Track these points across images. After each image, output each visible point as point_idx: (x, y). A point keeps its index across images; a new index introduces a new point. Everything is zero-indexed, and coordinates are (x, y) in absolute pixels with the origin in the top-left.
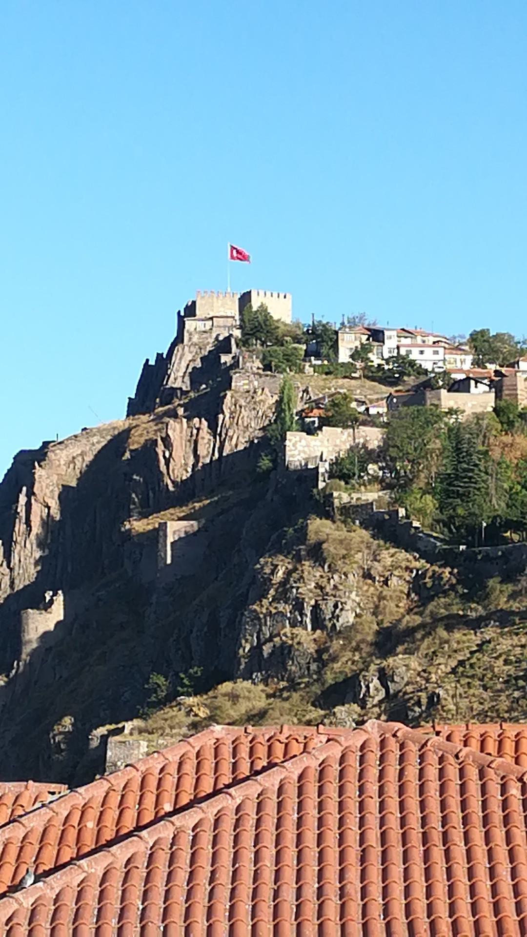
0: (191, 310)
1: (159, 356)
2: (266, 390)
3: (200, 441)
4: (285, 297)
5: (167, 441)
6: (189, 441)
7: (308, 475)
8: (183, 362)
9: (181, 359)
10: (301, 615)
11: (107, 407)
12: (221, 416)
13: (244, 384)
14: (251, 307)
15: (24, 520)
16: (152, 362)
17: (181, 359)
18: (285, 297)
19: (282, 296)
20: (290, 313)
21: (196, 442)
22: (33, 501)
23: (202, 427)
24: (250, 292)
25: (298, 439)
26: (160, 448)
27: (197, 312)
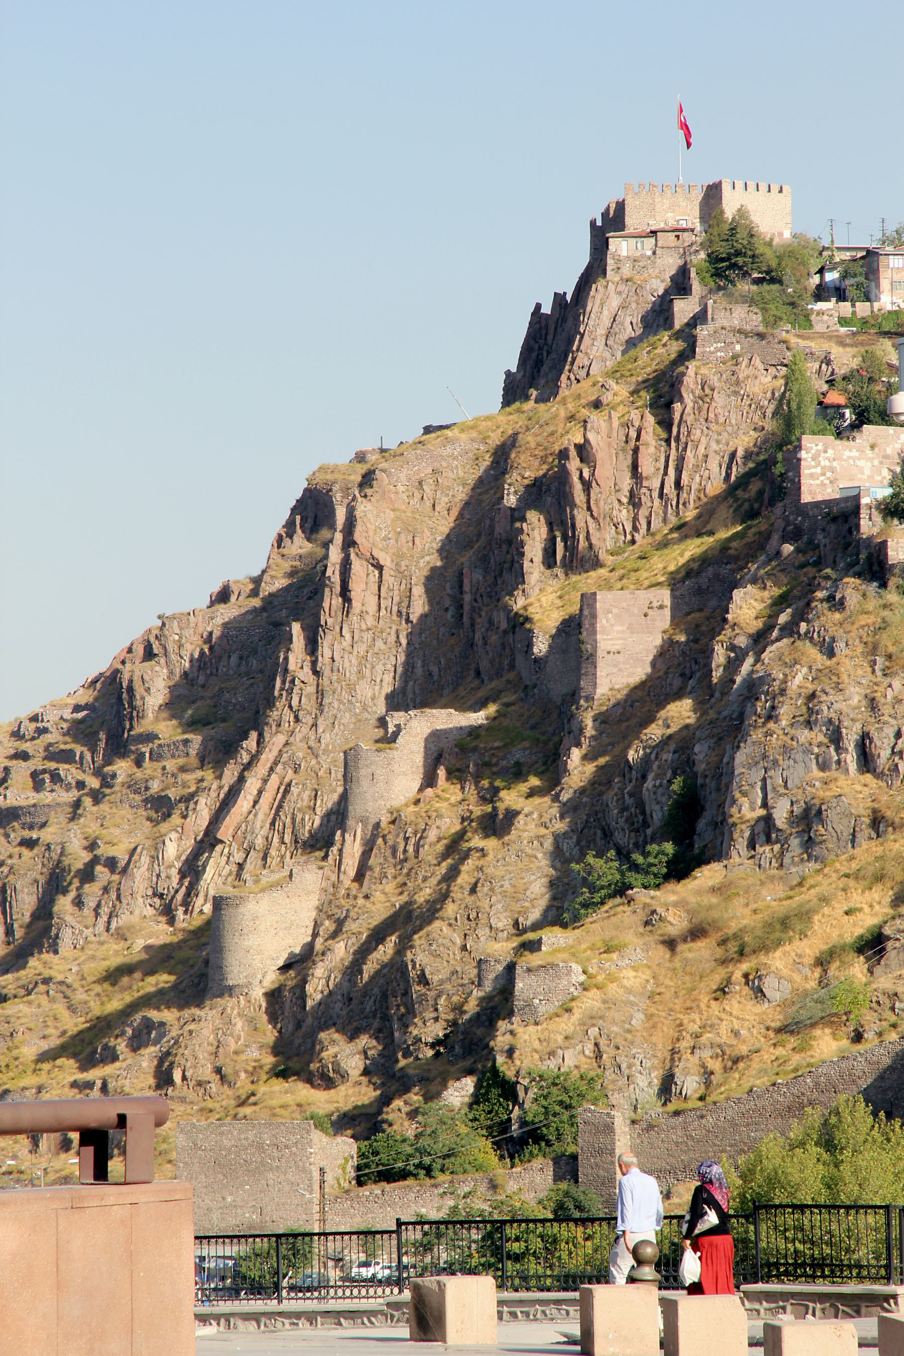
0: (613, 221)
1: (559, 298)
2: (757, 361)
3: (642, 449)
4: (781, 191)
5: (583, 451)
6: (624, 450)
7: (845, 513)
8: (605, 312)
9: (602, 305)
10: (838, 749)
11: (465, 380)
12: (677, 406)
13: (718, 350)
14: (722, 212)
15: (338, 589)
16: (546, 309)
17: (602, 305)
18: (781, 191)
19: (775, 188)
20: (789, 219)
21: (636, 450)
22: (353, 556)
23: (646, 424)
24: (720, 182)
25: (820, 447)
26: (574, 464)
27: (628, 221)
